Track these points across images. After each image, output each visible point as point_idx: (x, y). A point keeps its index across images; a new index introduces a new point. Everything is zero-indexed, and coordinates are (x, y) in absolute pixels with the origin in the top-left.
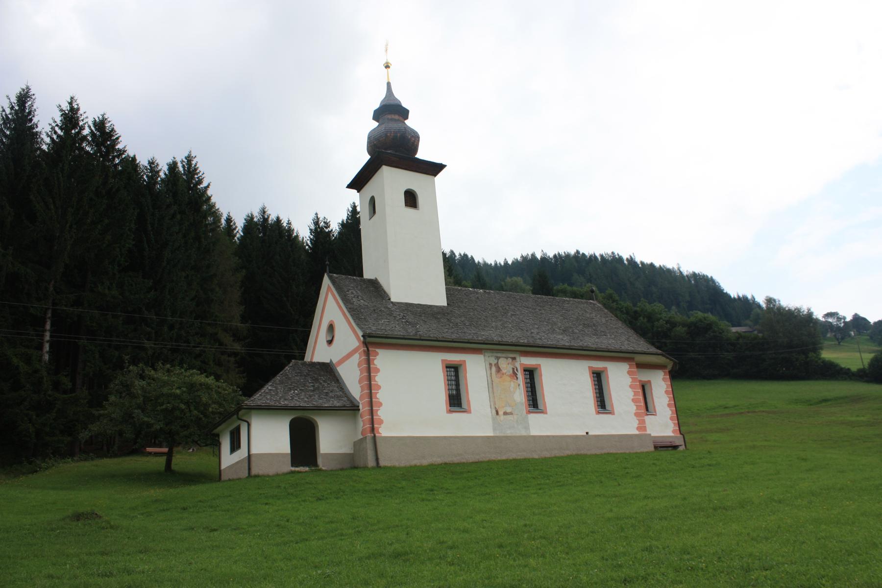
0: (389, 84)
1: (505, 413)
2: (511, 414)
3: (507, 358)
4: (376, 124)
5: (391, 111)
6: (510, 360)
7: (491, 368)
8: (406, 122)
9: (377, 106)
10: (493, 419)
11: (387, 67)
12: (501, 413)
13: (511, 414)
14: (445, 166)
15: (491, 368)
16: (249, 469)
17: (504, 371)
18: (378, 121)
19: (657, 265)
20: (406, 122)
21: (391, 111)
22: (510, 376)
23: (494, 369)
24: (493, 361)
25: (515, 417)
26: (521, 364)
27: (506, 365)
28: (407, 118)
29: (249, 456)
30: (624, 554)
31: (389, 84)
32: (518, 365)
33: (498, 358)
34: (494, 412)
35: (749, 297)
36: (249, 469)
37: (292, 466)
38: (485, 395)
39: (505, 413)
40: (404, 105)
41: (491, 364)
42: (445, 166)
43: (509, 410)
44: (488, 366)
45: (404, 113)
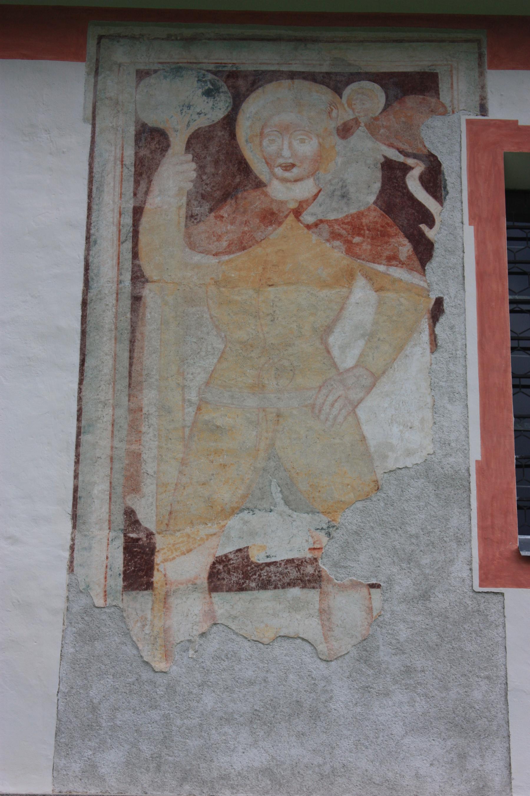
1: (233, 574)
2: (303, 575)
3: (335, 82)
6: (370, 99)
7: (144, 171)
10: (83, 625)
12: (181, 565)
13: (303, 575)
15: (144, 171)
17: (283, 192)
22: (349, 232)
23: (176, 176)
24: (183, 106)
25: (349, 608)
26: (482, 133)
27: (309, 143)
30: (313, 395)
32: (448, 138)
33: (239, 85)
34: (106, 554)
37: (520, 533)
38: (473, 555)
39: (233, 574)
41: (151, 141)
43: (279, 539)
44: (119, 150)
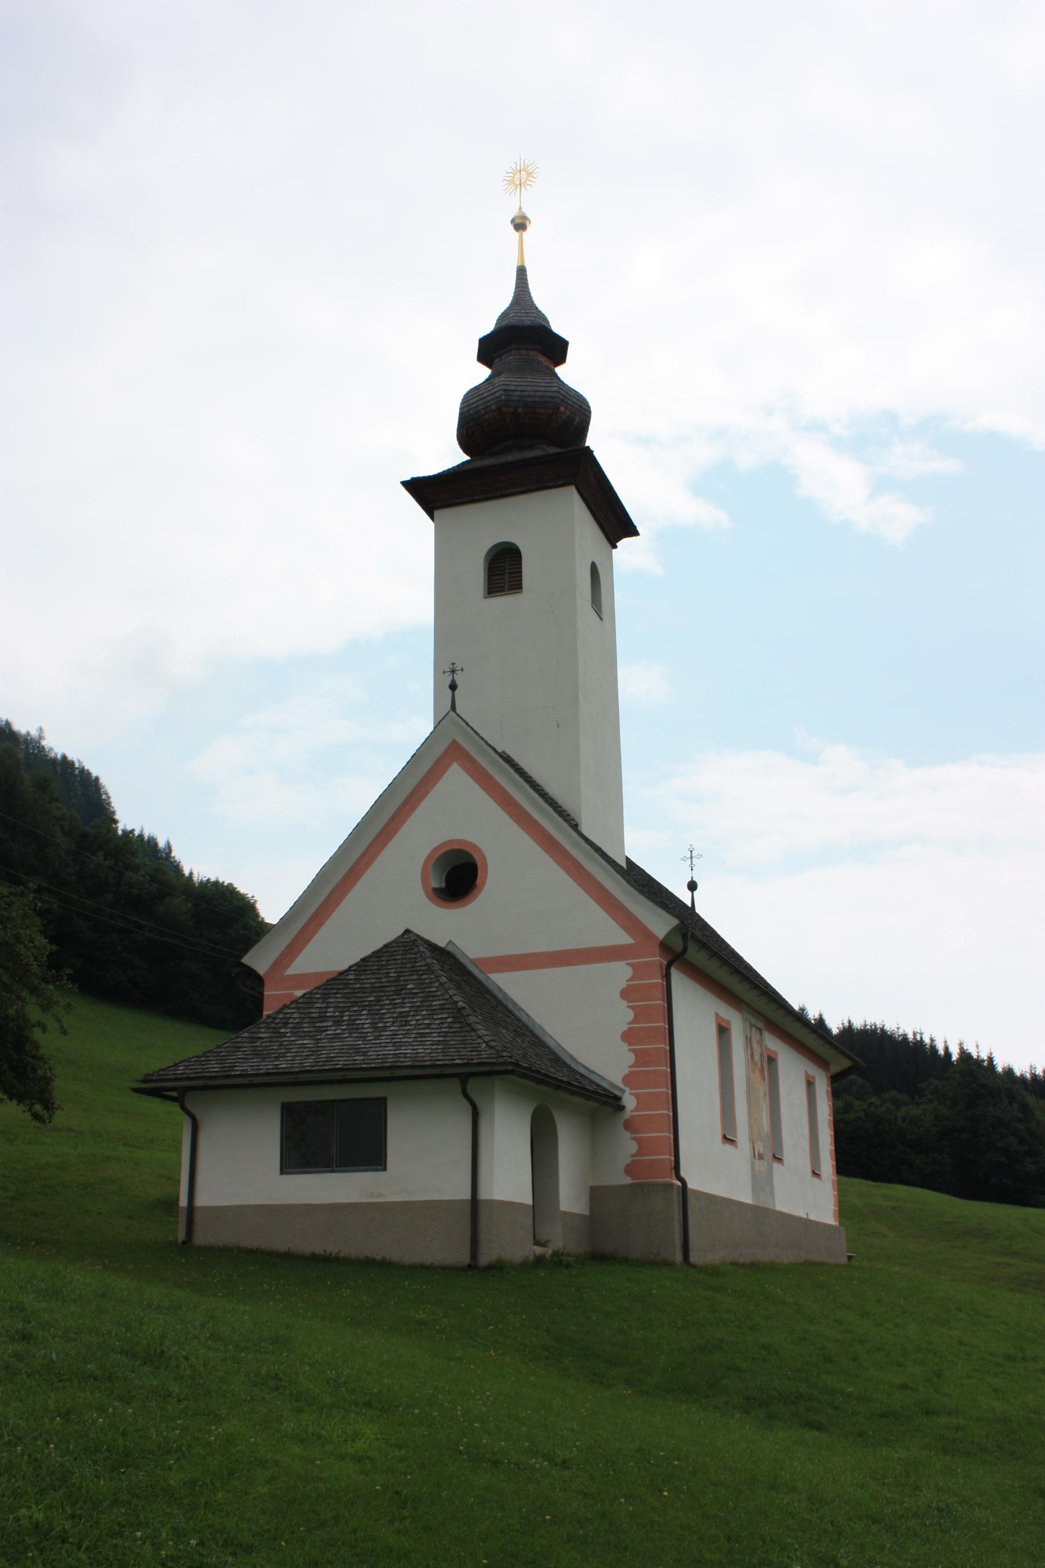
0: (522, 273)
4: (484, 372)
5: (523, 343)
8: (560, 371)
9: (488, 327)
11: (520, 225)
14: (405, 484)
16: (474, 1241)
18: (489, 366)
19: (858, 1024)
20: (560, 371)
21: (523, 343)
28: (561, 359)
29: (475, 1201)
31: (522, 273)
35: (162, 844)
36: (474, 1241)
40: (558, 327)
42: (405, 484)
45: (556, 349)
